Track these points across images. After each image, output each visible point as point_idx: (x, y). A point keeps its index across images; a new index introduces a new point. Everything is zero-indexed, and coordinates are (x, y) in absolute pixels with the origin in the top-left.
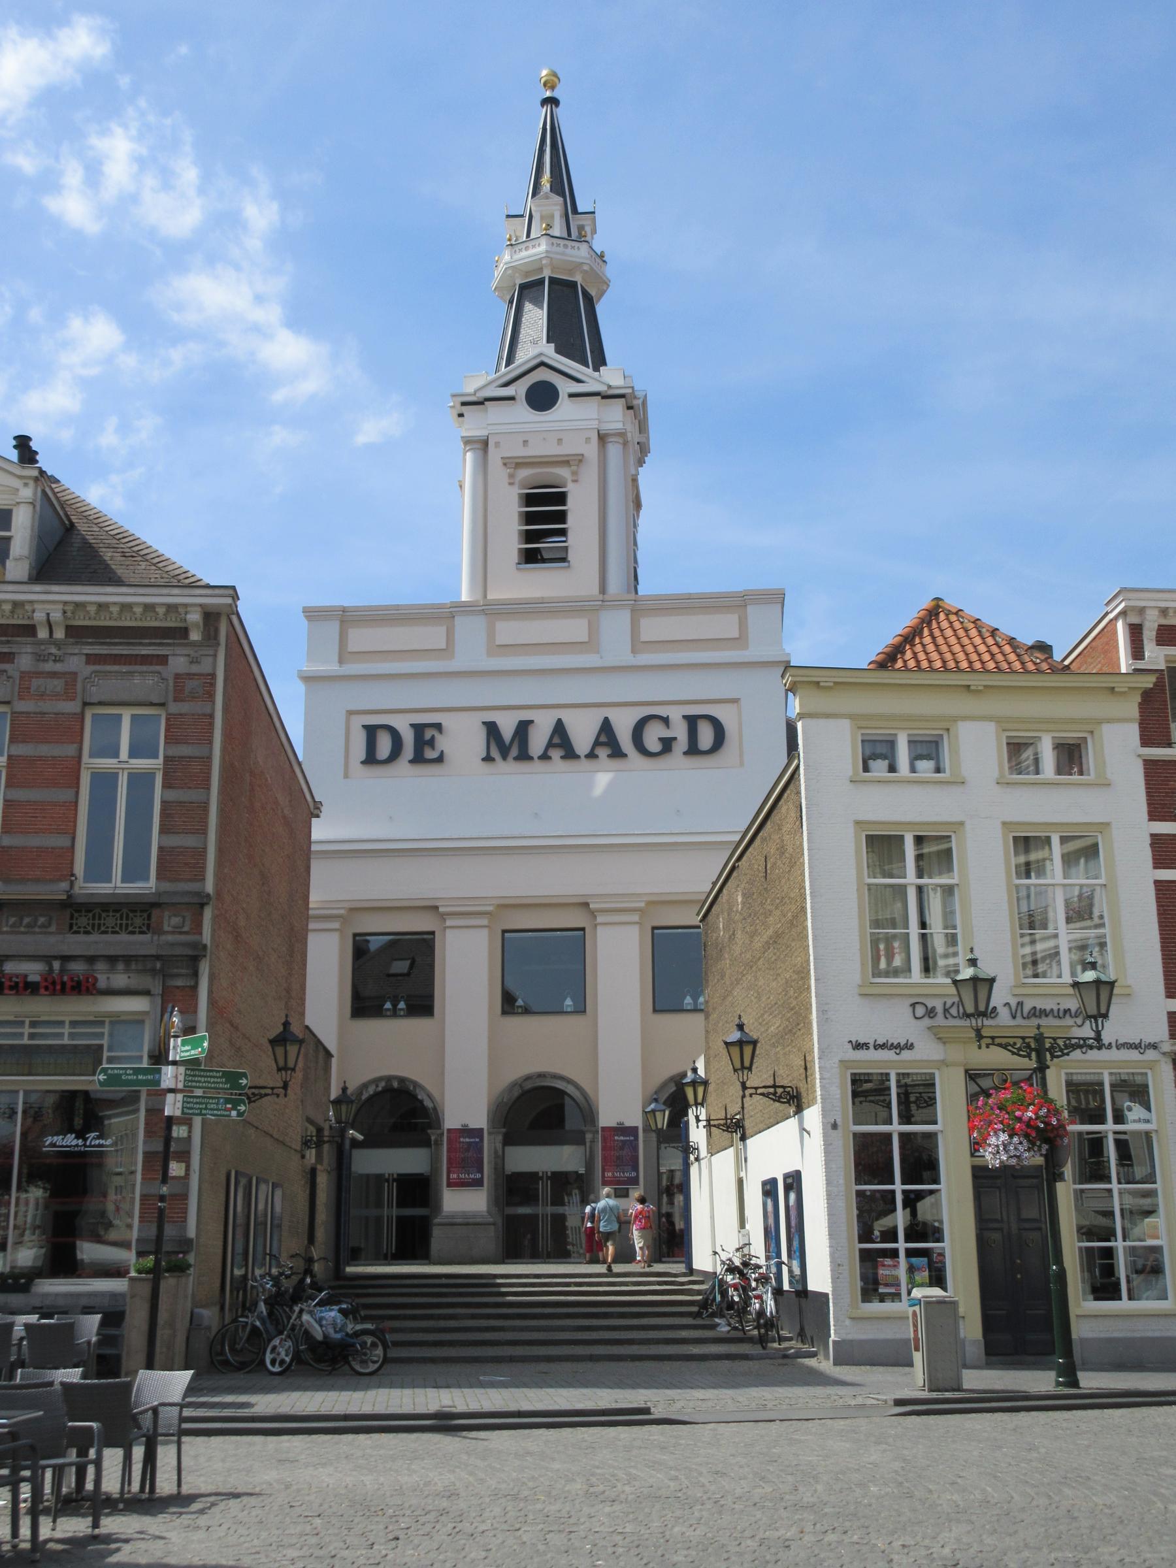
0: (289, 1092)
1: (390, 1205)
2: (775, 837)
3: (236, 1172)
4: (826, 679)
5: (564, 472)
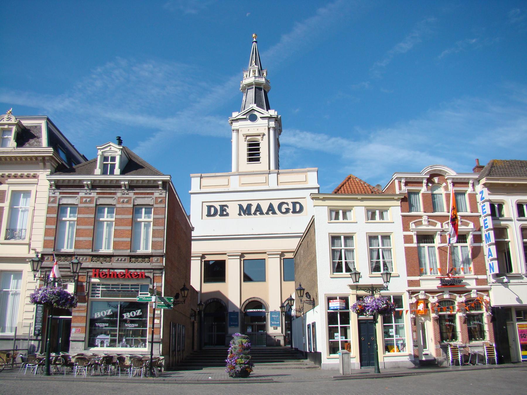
2: (310, 237)
5: (259, 138)
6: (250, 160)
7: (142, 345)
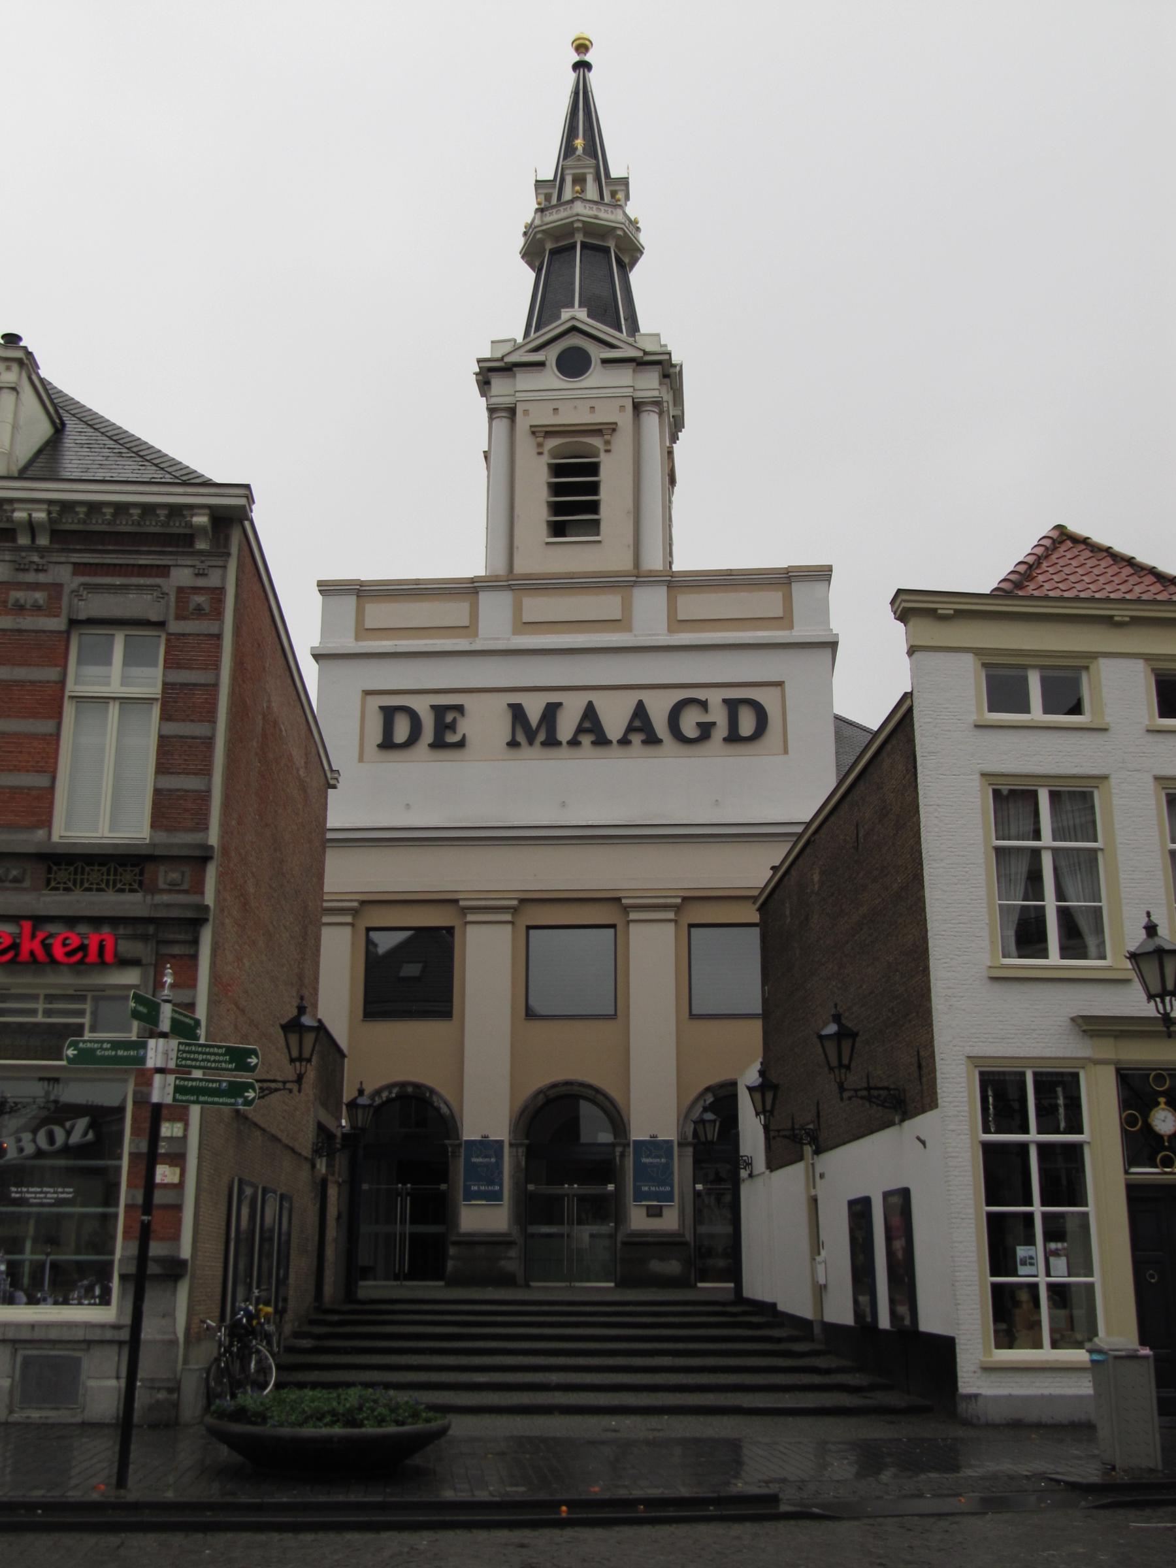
0: (303, 1086)
1: (403, 1222)
3: (241, 1181)
4: (946, 609)
5: (596, 442)
6: (558, 529)
7: (89, 1290)
